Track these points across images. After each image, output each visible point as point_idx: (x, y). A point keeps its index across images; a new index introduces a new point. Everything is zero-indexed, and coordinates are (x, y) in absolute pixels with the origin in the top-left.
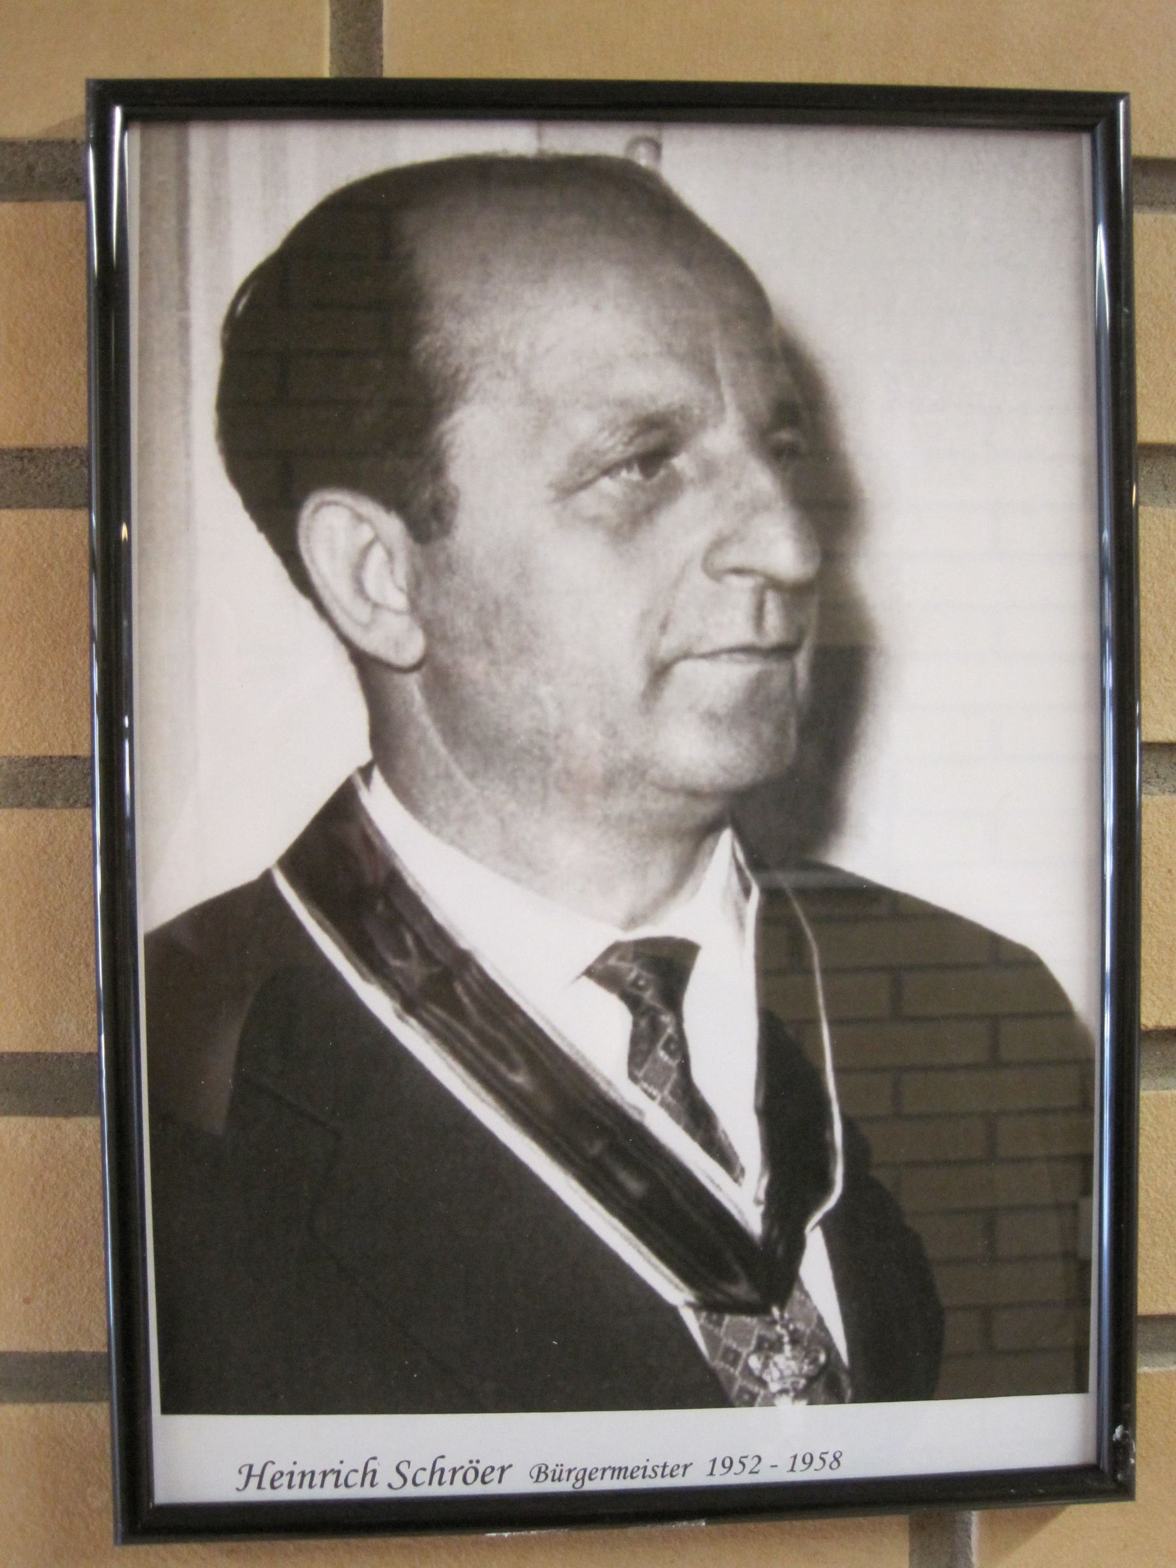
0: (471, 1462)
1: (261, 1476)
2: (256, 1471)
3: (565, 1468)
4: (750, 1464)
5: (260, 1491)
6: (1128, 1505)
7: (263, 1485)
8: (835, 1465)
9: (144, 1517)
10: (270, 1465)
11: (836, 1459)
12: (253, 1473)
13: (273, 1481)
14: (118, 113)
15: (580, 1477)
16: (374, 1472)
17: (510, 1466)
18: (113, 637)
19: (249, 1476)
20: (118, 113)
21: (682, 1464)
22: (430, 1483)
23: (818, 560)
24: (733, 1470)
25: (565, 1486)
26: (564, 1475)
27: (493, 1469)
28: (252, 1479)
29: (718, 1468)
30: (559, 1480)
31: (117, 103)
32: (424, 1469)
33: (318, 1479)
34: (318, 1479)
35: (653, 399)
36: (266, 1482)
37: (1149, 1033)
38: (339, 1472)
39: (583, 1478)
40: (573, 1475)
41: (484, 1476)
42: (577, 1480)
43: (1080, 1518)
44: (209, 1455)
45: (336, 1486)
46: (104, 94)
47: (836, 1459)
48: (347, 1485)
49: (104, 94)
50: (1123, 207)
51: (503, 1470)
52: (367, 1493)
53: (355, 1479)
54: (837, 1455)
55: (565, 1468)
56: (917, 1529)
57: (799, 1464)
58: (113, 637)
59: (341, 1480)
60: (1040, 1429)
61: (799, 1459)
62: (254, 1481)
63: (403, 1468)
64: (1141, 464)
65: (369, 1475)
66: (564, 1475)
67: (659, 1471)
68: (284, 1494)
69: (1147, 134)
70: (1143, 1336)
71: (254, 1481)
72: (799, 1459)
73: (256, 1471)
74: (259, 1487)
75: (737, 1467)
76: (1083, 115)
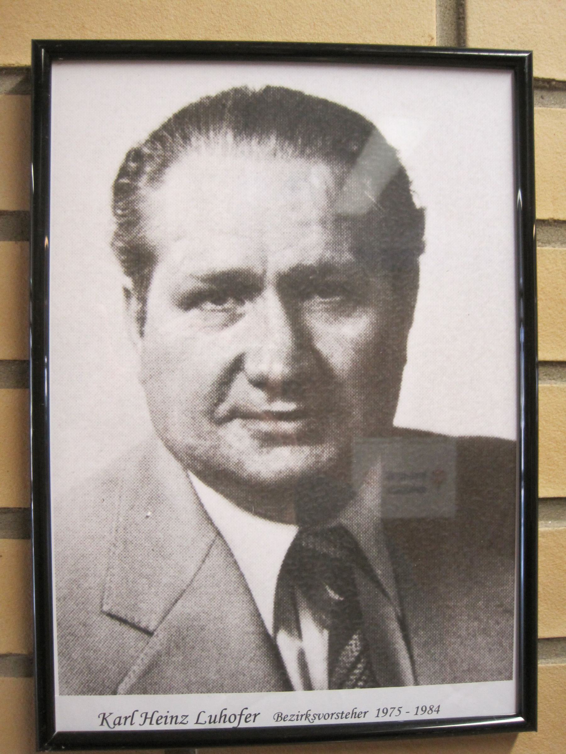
1: (152, 718)
2: (149, 716)
5: (151, 726)
6: (534, 733)
8: (430, 712)
11: (431, 709)
12: (148, 717)
13: (157, 720)
17: (259, 714)
19: (146, 718)
21: (123, 716)
28: (147, 720)
29: (381, 714)
30: (214, 722)
35: (13, 65)
43: (523, 736)
47: (431, 709)
50: (452, 53)
54: (432, 707)
56: (24, 512)
57: (420, 711)
61: (381, 711)
62: (148, 721)
67: (340, 715)
68: (162, 727)
69: (539, 71)
70: (541, 649)
71: (148, 721)
73: (149, 716)
74: (151, 724)
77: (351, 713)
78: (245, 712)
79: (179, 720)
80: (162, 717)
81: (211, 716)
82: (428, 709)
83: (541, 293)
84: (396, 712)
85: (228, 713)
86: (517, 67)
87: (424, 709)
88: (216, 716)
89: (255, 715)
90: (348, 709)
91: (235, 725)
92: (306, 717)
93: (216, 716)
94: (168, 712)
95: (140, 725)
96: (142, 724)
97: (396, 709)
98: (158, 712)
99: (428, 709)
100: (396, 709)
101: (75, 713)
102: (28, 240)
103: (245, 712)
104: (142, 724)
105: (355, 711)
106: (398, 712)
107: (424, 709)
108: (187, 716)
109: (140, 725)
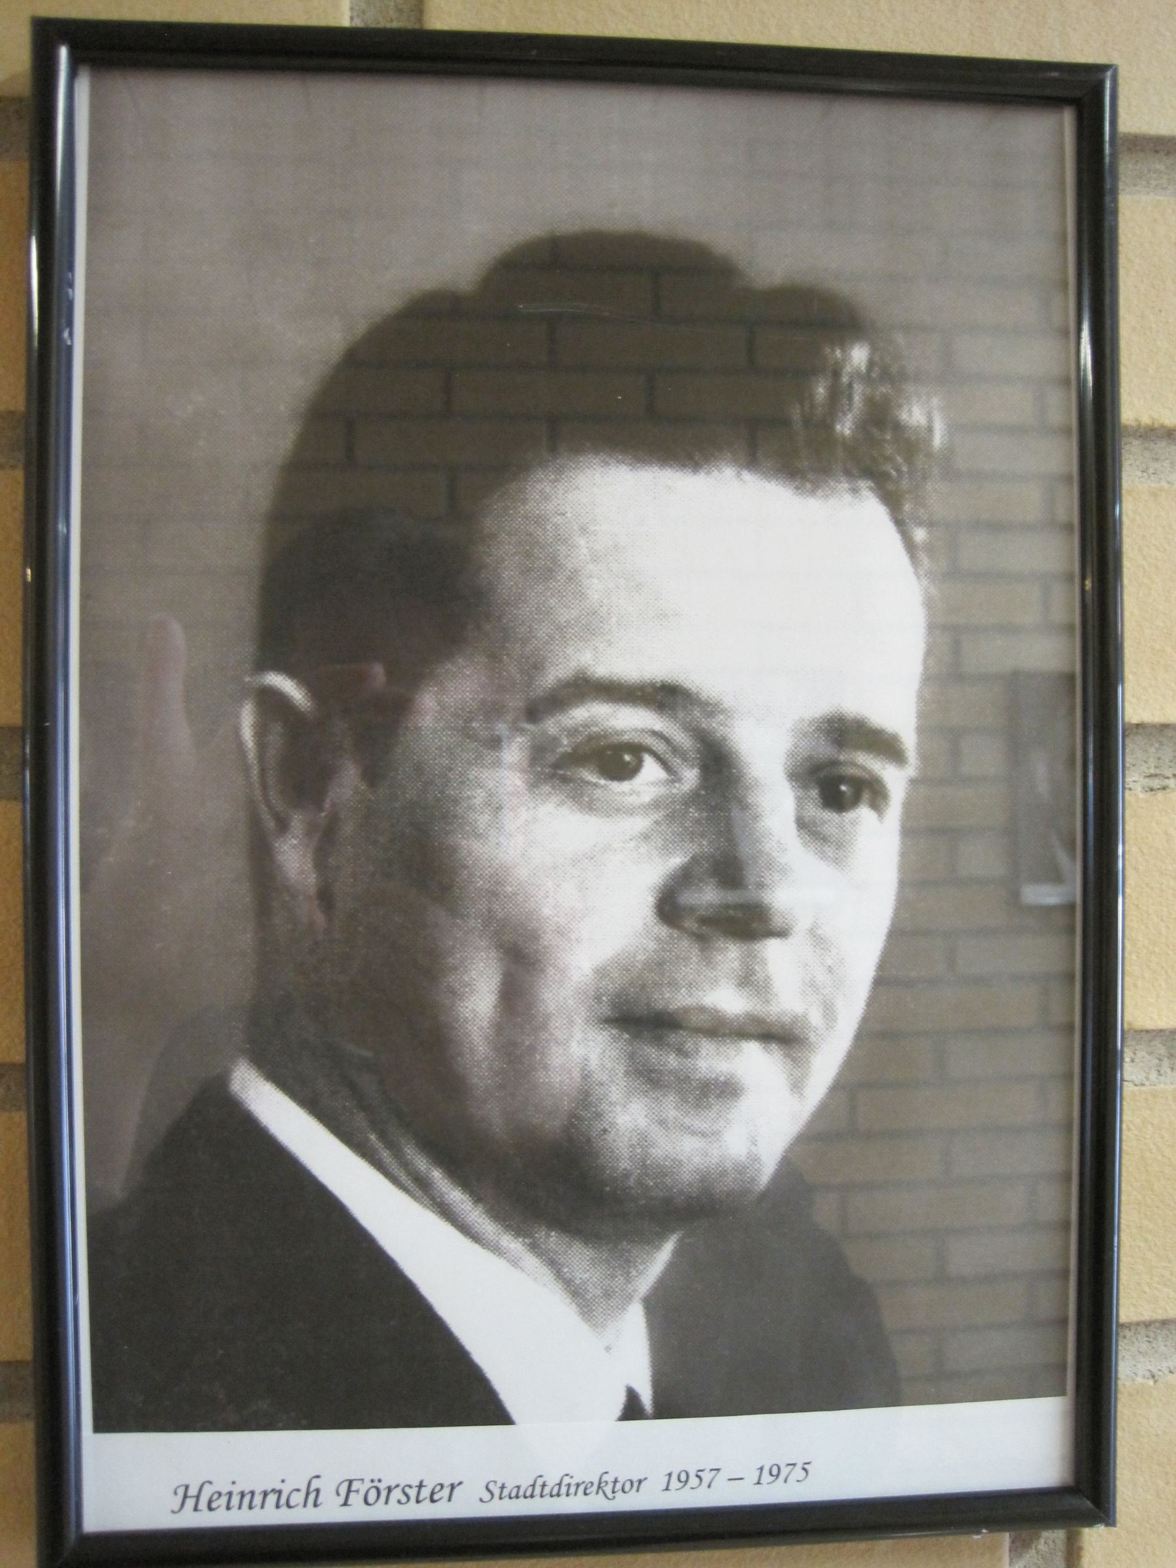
0: (372, 1481)
1: (198, 1497)
2: (193, 1491)
7: (200, 1507)
13: (210, 1502)
14: (63, 53)
16: (318, 1491)
17: (460, 1483)
19: (185, 1497)
20: (63, 53)
21: (447, 1483)
22: (305, 1505)
23: (864, 485)
24: (690, 1484)
27: (442, 1486)
28: (188, 1500)
31: (63, 44)
32: (298, 1490)
33: (258, 1499)
34: (258, 1499)
36: (203, 1504)
37: (1128, 1326)
38: (280, 1492)
44: (136, 1480)
45: (278, 1506)
46: (48, 34)
49: (48, 34)
51: (453, 1487)
55: (573, 1482)
59: (283, 1501)
60: (1012, 1441)
61: (674, 1477)
62: (190, 1503)
63: (491, 1486)
65: (313, 1495)
67: (413, 1493)
71: (190, 1503)
72: (674, 1477)
73: (193, 1491)
74: (196, 1509)
75: (693, 1481)
76: (1077, 93)
80: (220, 1494)
83: (1130, 498)
84: (798, 1473)
89: (640, 1482)
92: (599, 1487)
94: (234, 1483)
95: (173, 1512)
96: (176, 1509)
97: (799, 1466)
98: (210, 1483)
101: (136, 1480)
103: (566, 1480)
104: (176, 1509)
106: (697, 1480)
108: (718, 1470)
109: (173, 1512)
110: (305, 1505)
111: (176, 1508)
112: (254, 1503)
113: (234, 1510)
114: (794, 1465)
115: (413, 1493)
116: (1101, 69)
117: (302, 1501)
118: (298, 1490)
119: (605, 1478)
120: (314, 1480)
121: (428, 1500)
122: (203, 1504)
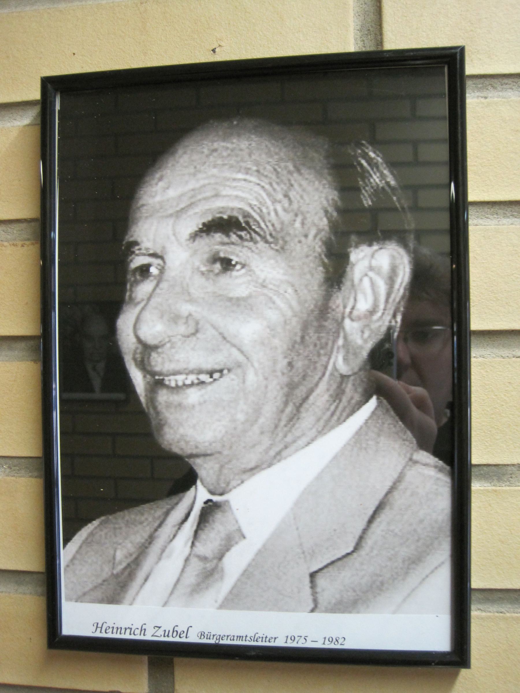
1: (101, 628)
2: (100, 625)
3: (212, 634)
4: (340, 641)
8: (336, 643)
9: (57, 641)
10: (190, 628)
11: (337, 640)
13: (106, 630)
15: (218, 638)
16: (145, 630)
18: (456, 374)
19: (97, 627)
22: (140, 635)
25: (212, 641)
26: (212, 637)
27: (109, 627)
30: (209, 639)
32: (138, 629)
33: (123, 631)
34: (123, 631)
36: (103, 631)
38: (131, 629)
39: (219, 639)
40: (215, 637)
41: (222, 637)
42: (217, 639)
45: (130, 634)
47: (337, 640)
48: (134, 634)
52: (142, 637)
53: (137, 632)
55: (212, 634)
56: (152, 665)
57: (327, 642)
58: (456, 374)
59: (132, 632)
61: (289, 638)
62: (99, 630)
64: (467, 81)
65: (143, 630)
66: (212, 637)
71: (99, 630)
72: (289, 638)
73: (100, 625)
74: (101, 632)
77: (140, 629)
78: (257, 636)
79: (248, 638)
81: (165, 631)
82: (334, 640)
85: (179, 629)
86: (459, 655)
87: (331, 640)
88: (169, 631)
89: (275, 638)
90: (251, 634)
91: (217, 642)
93: (169, 631)
97: (303, 638)
99: (334, 640)
100: (303, 638)
102: (172, 659)
103: (257, 636)
105: (144, 627)
107: (331, 640)
110: (140, 635)
111: (94, 631)
112: (122, 632)
113: (264, 642)
114: (301, 636)
115: (252, 638)
116: (462, 50)
117: (139, 633)
118: (138, 629)
119: (176, 629)
120: (144, 626)
121: (171, 637)
122: (103, 631)
